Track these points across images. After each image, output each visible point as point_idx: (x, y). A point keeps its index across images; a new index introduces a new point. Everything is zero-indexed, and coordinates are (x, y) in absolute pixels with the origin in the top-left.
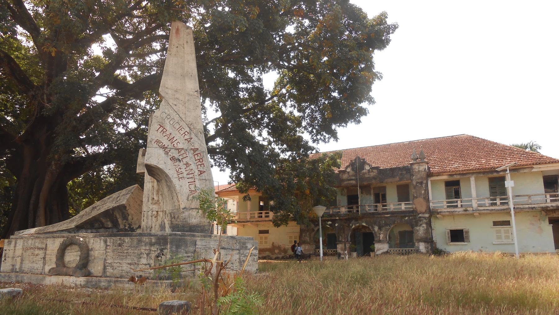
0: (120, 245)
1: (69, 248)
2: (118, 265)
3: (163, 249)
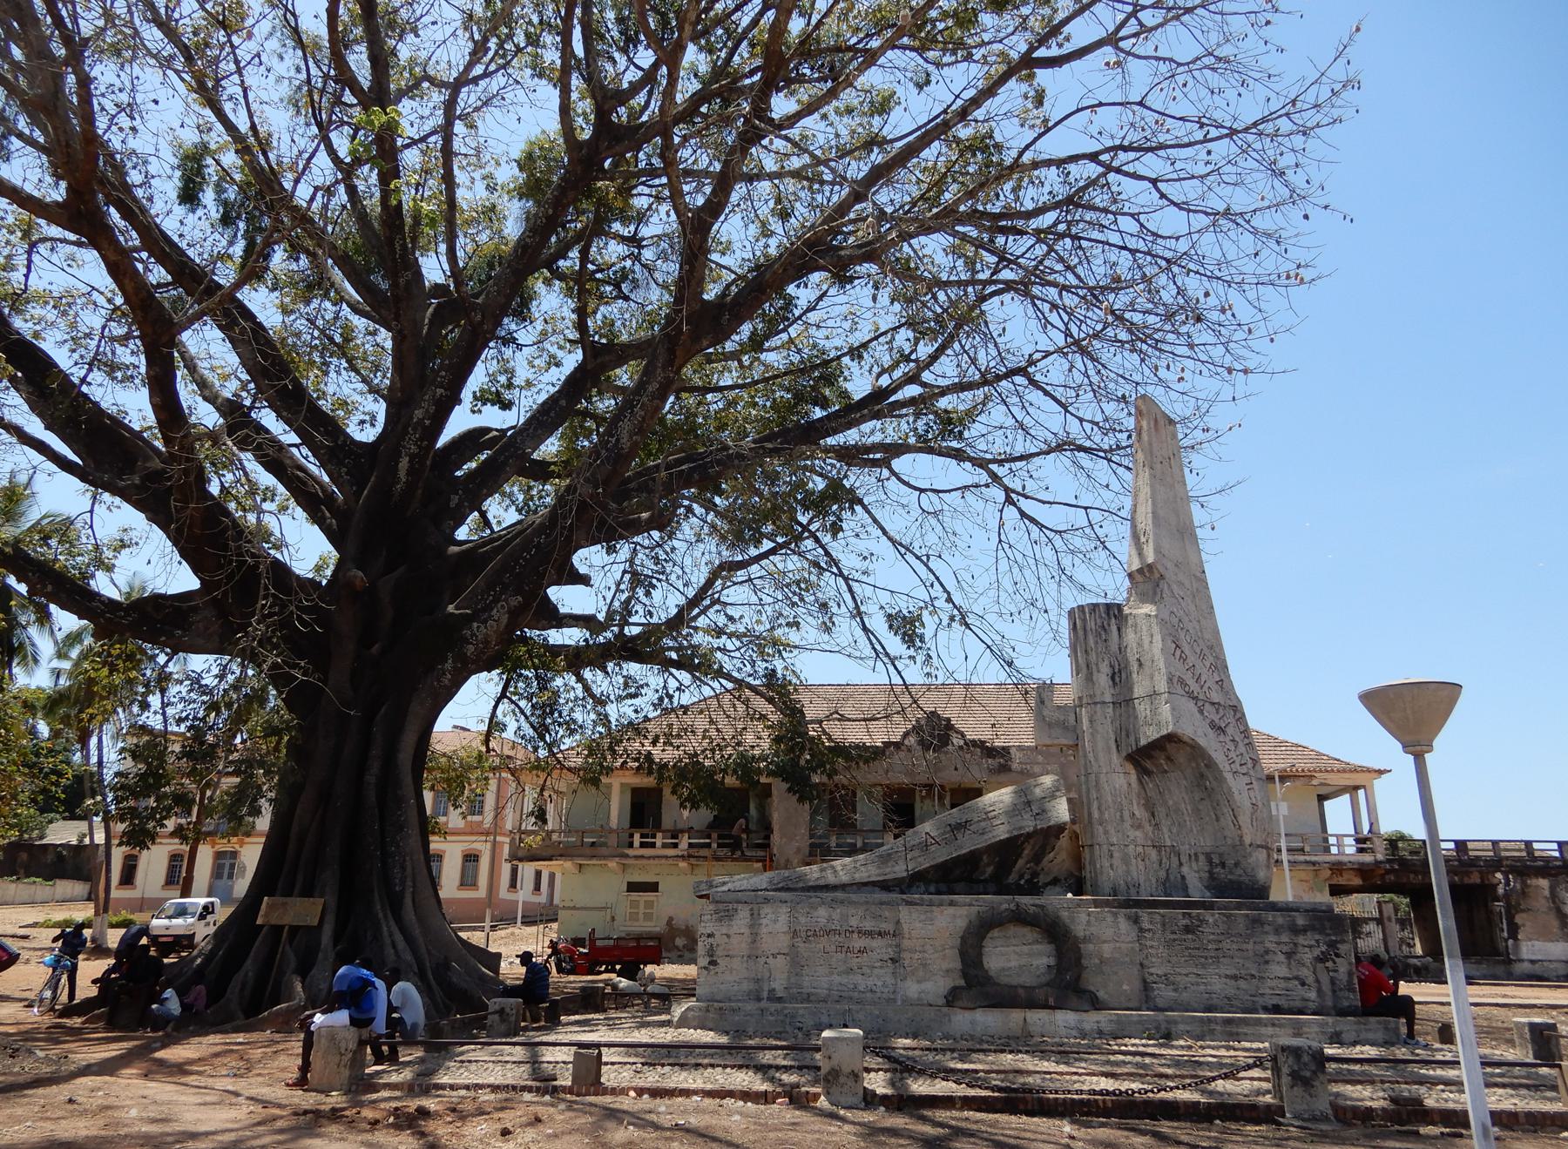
0: (1188, 930)
1: (995, 933)
2: (1192, 978)
3: (1336, 942)
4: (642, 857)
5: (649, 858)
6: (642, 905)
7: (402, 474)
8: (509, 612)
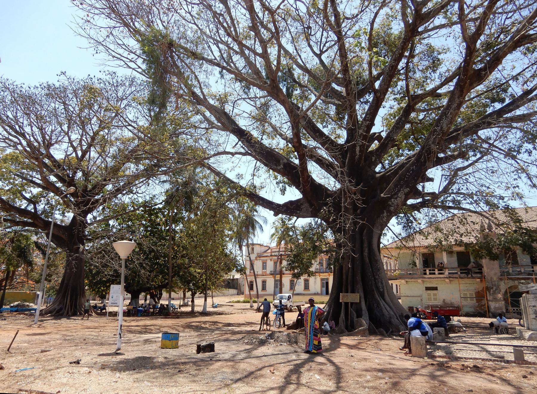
4: (431, 278)
5: (434, 278)
6: (432, 295)
7: (358, 152)
8: (405, 194)
